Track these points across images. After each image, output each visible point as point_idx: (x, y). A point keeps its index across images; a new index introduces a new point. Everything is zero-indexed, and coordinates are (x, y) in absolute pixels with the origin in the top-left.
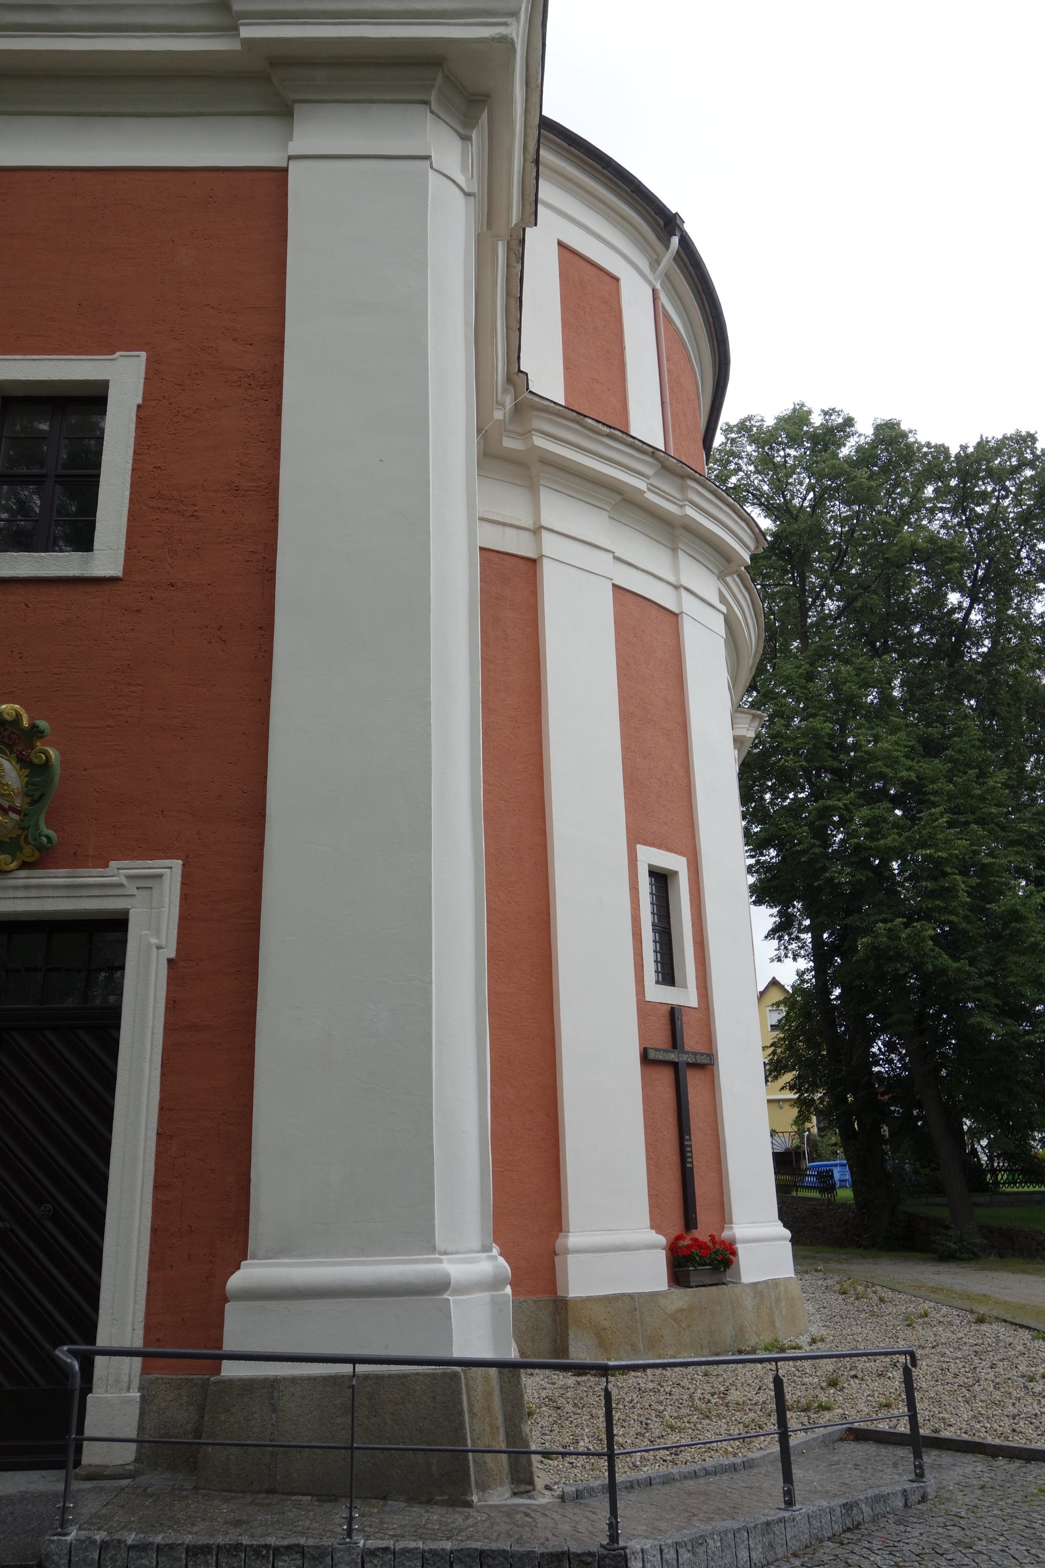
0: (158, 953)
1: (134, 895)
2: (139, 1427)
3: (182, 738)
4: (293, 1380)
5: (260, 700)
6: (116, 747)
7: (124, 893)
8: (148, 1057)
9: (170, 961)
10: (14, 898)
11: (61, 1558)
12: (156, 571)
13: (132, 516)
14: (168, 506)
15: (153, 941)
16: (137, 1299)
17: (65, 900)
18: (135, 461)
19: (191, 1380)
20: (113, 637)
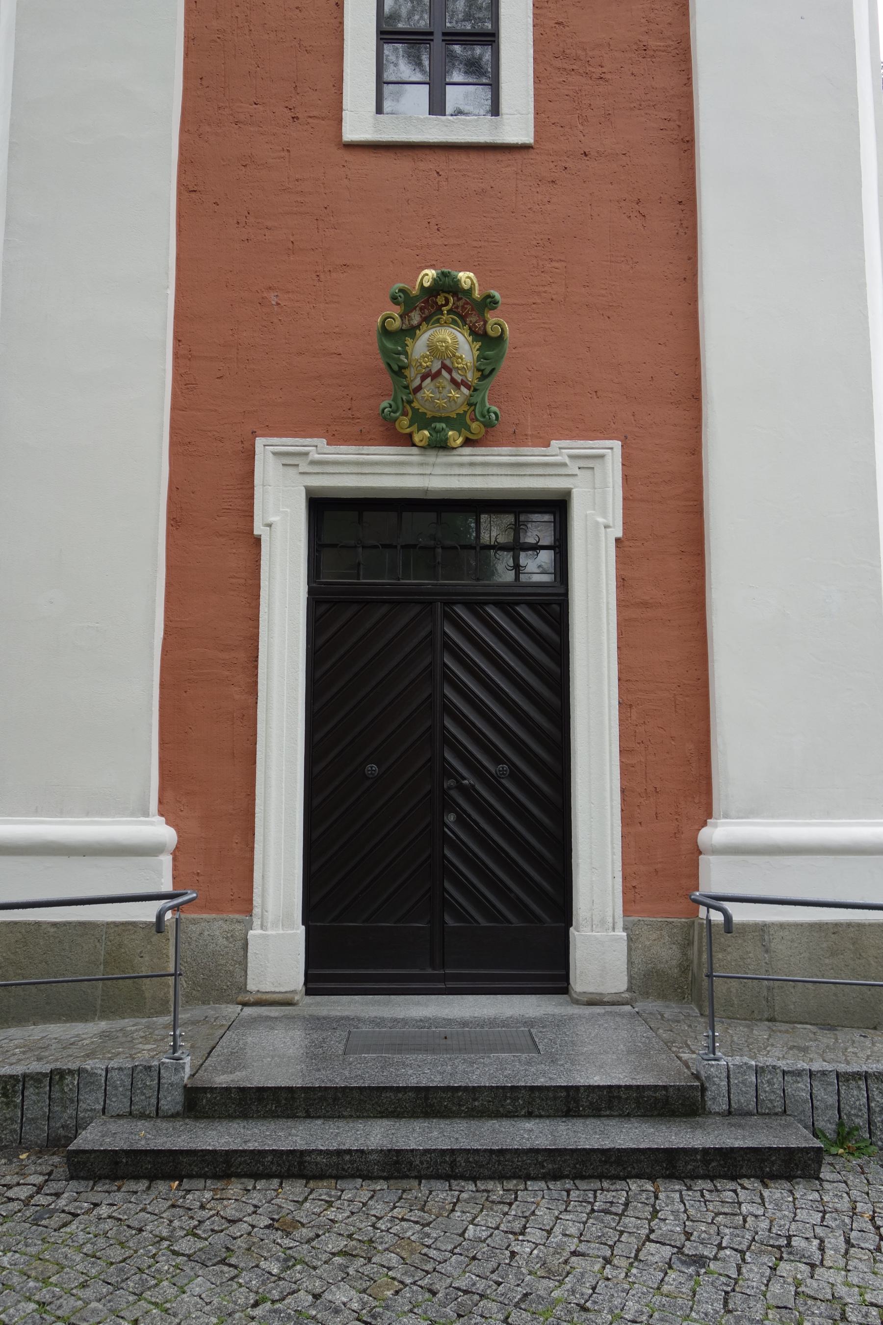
0: (606, 533)
1: (576, 475)
2: (628, 961)
3: (609, 318)
4: (782, 926)
5: (685, 279)
6: (543, 325)
7: (567, 473)
8: (605, 630)
9: (618, 540)
10: (459, 475)
11: (721, 1080)
12: (568, 139)
13: (538, 79)
14: (575, 67)
15: (601, 520)
16: (615, 850)
17: (509, 478)
18: (535, 15)
19: (671, 923)
20: (530, 209)
